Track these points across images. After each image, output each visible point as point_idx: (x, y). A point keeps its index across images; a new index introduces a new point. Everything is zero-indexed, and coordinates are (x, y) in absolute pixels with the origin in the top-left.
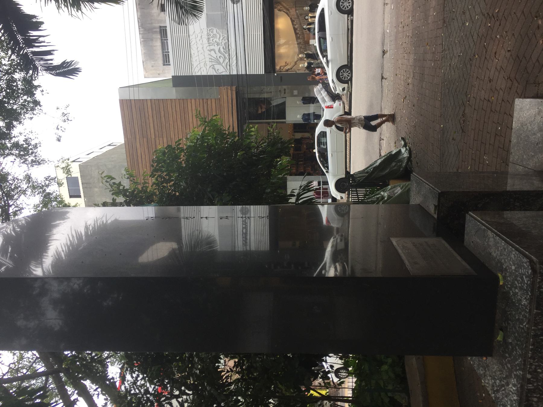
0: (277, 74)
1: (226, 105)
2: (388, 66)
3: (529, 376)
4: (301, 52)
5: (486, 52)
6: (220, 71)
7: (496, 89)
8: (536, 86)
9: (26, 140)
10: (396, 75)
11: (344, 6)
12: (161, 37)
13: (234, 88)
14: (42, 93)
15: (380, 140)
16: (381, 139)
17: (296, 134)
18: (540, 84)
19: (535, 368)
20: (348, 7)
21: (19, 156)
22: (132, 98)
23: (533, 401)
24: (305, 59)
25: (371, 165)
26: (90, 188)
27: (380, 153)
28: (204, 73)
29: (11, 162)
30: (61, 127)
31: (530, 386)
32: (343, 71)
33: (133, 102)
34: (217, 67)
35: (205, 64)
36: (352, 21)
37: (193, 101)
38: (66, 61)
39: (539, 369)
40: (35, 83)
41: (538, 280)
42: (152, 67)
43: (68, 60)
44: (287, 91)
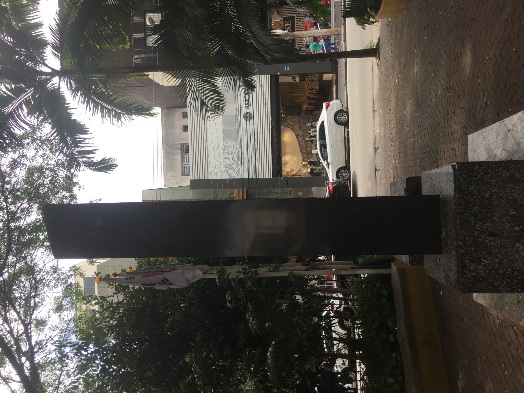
0: (284, 178)
2: (380, 158)
3: (461, 243)
4: (304, 160)
5: (448, 115)
6: (233, 176)
7: (457, 139)
8: (482, 125)
11: (341, 119)
12: (182, 152)
13: (245, 189)
14: (79, 189)
18: (485, 123)
19: (464, 237)
20: (344, 120)
23: (466, 262)
24: (308, 166)
28: (219, 177)
29: (41, 253)
31: (462, 251)
32: (342, 171)
34: (230, 172)
35: (220, 170)
36: (348, 132)
38: (106, 158)
39: (466, 237)
41: (457, 174)
42: (172, 177)
43: (107, 158)
44: (292, 192)
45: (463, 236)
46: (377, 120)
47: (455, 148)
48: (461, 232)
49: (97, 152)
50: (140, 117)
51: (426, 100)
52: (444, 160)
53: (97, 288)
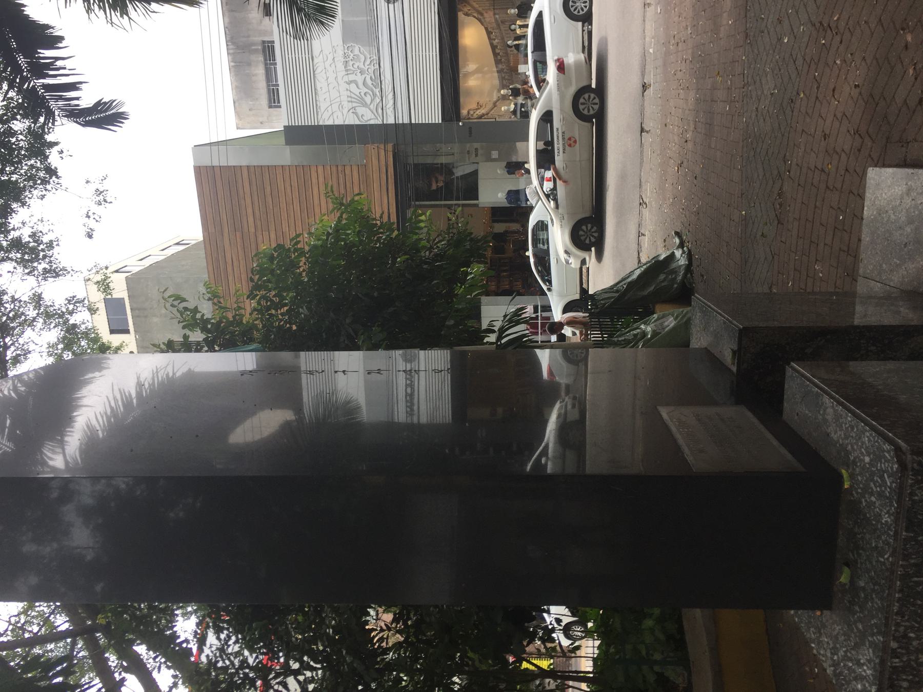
1: (376, 176)
2: (652, 109)
3: (894, 645)
4: (503, 87)
5: (818, 88)
6: (365, 118)
9: (33, 235)
10: (666, 125)
12: (265, 60)
13: (390, 147)
14: (61, 155)
15: (639, 236)
16: (640, 235)
17: (496, 225)
21: (22, 262)
22: (216, 163)
23: (901, 687)
24: (511, 98)
25: (623, 280)
26: (146, 317)
27: (639, 257)
30: (94, 213)
33: (217, 171)
34: (361, 110)
37: (320, 169)
38: (103, 101)
40: (49, 138)
41: (910, 481)
42: (250, 110)
43: (106, 100)
44: (480, 152)
45: (902, 629)
46: (650, 27)
47: (827, 170)
48: (899, 619)
49: (83, 86)
50: (167, 6)
51: (766, 31)
52: (799, 185)
53: (130, 310)
